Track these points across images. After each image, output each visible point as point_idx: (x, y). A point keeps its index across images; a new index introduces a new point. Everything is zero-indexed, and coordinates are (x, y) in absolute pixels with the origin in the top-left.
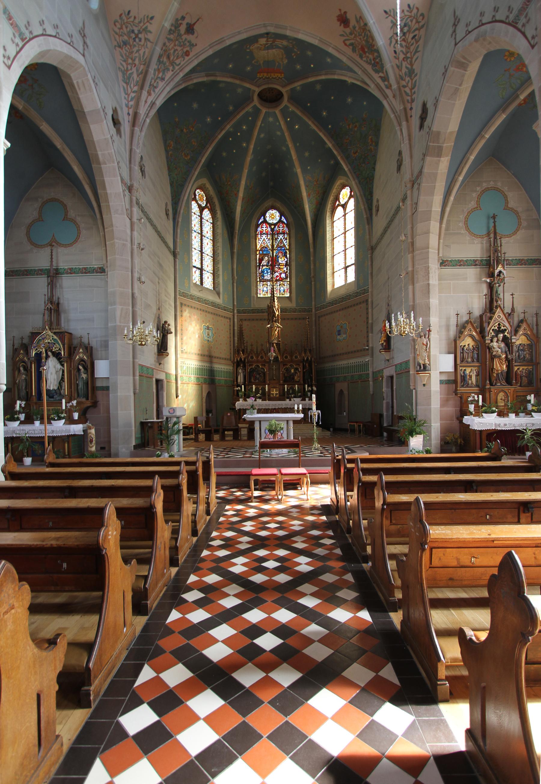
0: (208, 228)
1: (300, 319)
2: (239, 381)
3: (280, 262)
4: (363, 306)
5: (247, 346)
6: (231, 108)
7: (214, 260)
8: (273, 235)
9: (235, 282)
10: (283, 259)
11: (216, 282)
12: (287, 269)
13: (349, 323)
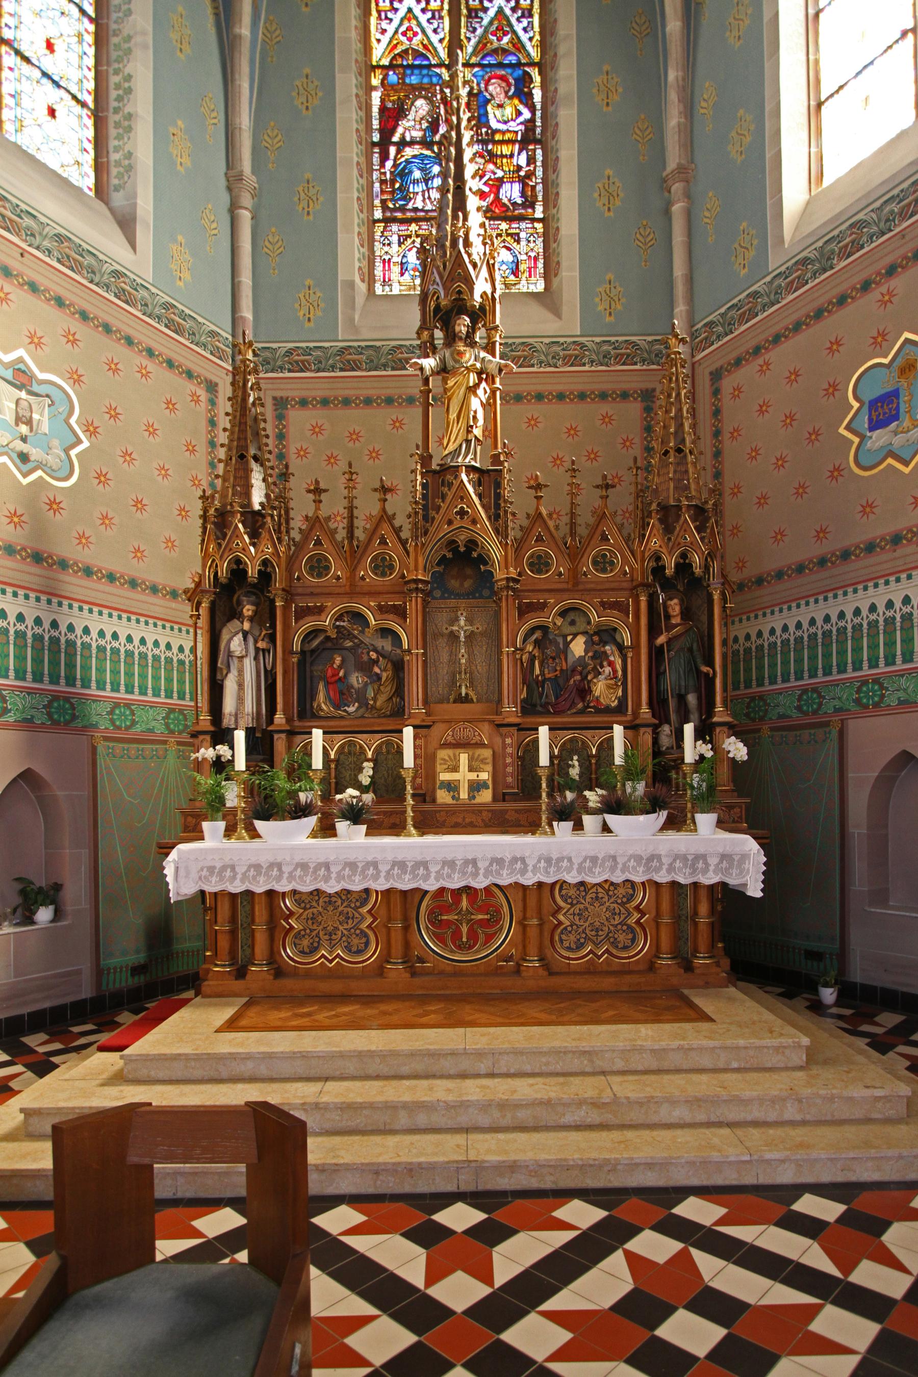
1: (603, 396)
2: (229, 705)
3: (494, 124)
7: (100, 41)
9: (246, 200)
10: (509, 111)
11: (114, 157)
12: (531, 160)
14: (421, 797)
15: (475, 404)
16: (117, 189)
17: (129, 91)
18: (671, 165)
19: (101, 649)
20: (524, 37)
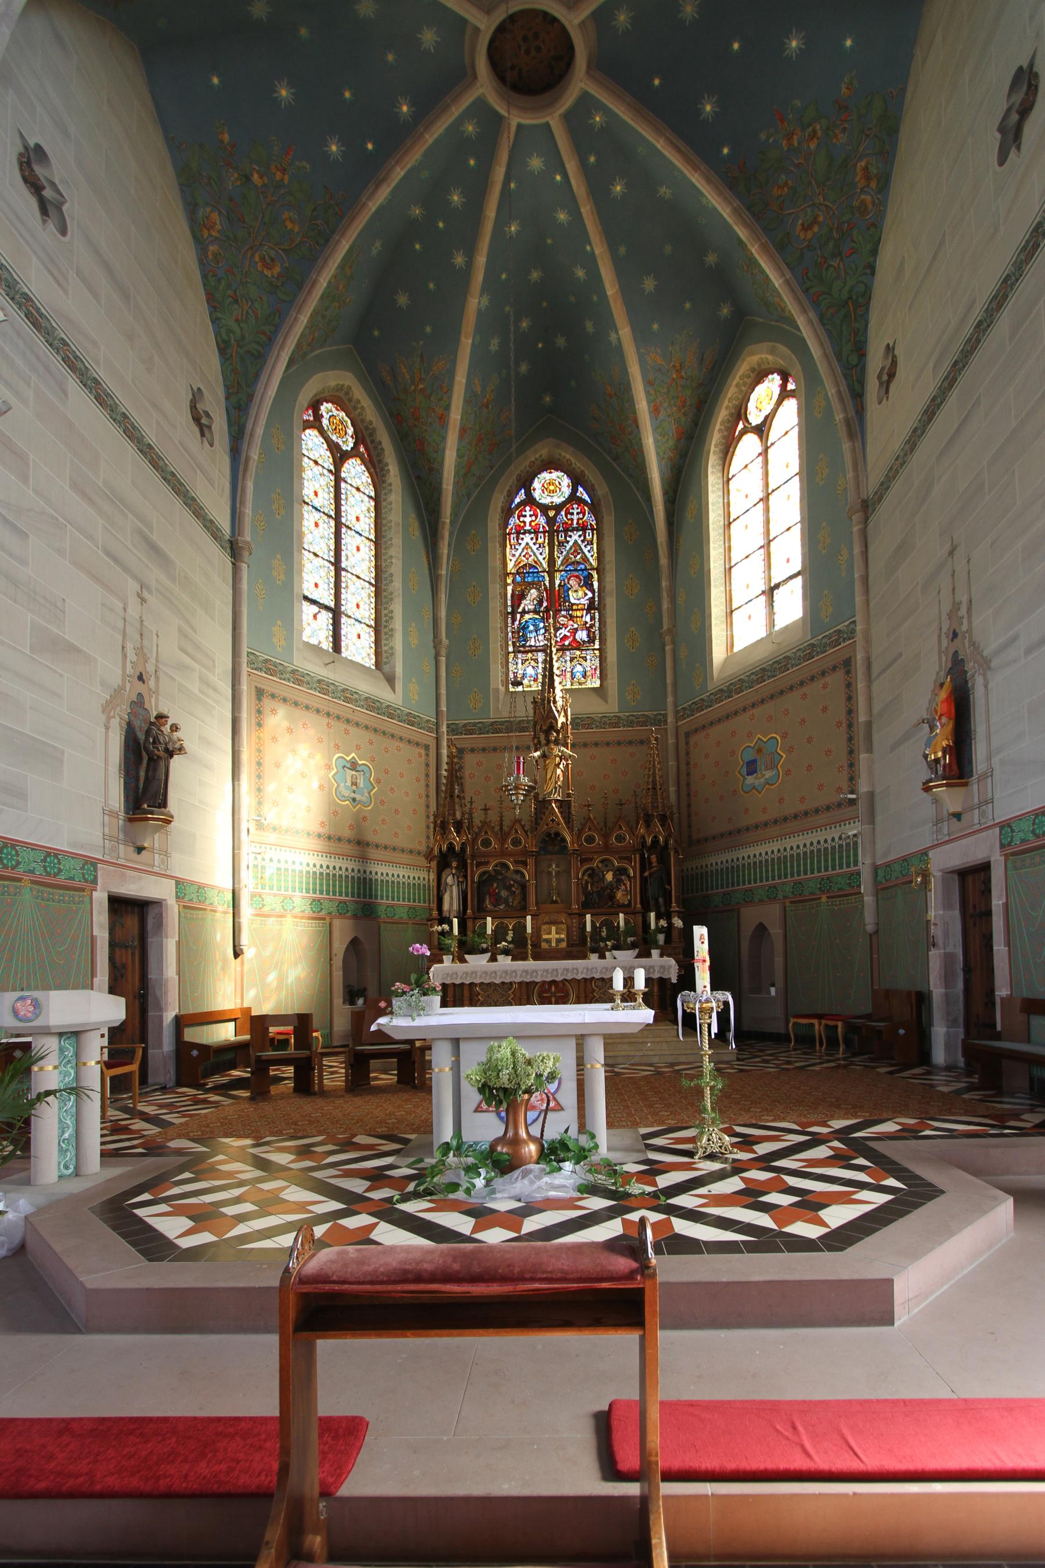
0: (359, 508)
1: (630, 743)
2: (446, 907)
3: (573, 601)
4: (836, 679)
5: (470, 814)
6: (405, 109)
7: (378, 594)
8: (552, 533)
9: (443, 652)
10: (580, 594)
11: (384, 648)
12: (592, 618)
13: (784, 736)
14: (534, 946)
15: (559, 771)
16: (386, 663)
17: (392, 618)
18: (665, 627)
19: (382, 881)
20: (589, 555)
